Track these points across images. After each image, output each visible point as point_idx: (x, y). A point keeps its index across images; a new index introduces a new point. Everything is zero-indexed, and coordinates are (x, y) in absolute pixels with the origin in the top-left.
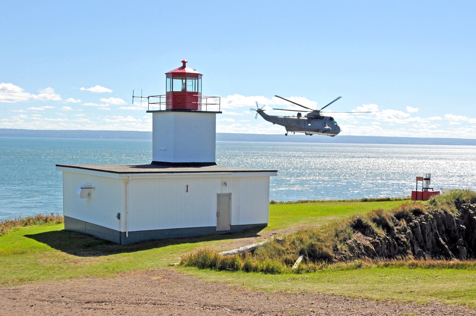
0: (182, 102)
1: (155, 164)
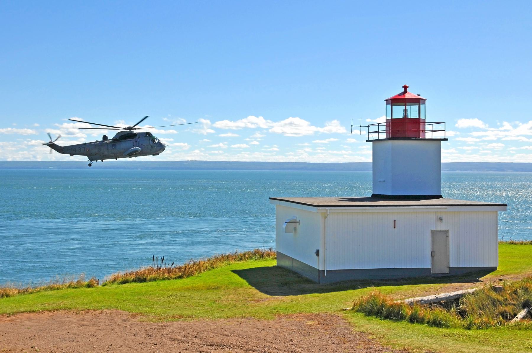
0: (404, 129)
1: (375, 197)
